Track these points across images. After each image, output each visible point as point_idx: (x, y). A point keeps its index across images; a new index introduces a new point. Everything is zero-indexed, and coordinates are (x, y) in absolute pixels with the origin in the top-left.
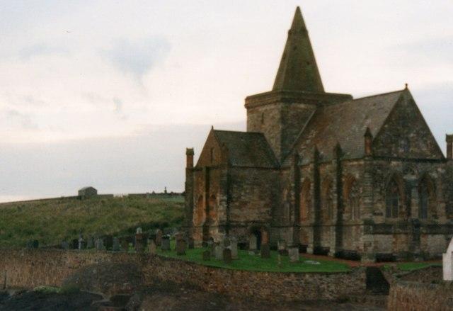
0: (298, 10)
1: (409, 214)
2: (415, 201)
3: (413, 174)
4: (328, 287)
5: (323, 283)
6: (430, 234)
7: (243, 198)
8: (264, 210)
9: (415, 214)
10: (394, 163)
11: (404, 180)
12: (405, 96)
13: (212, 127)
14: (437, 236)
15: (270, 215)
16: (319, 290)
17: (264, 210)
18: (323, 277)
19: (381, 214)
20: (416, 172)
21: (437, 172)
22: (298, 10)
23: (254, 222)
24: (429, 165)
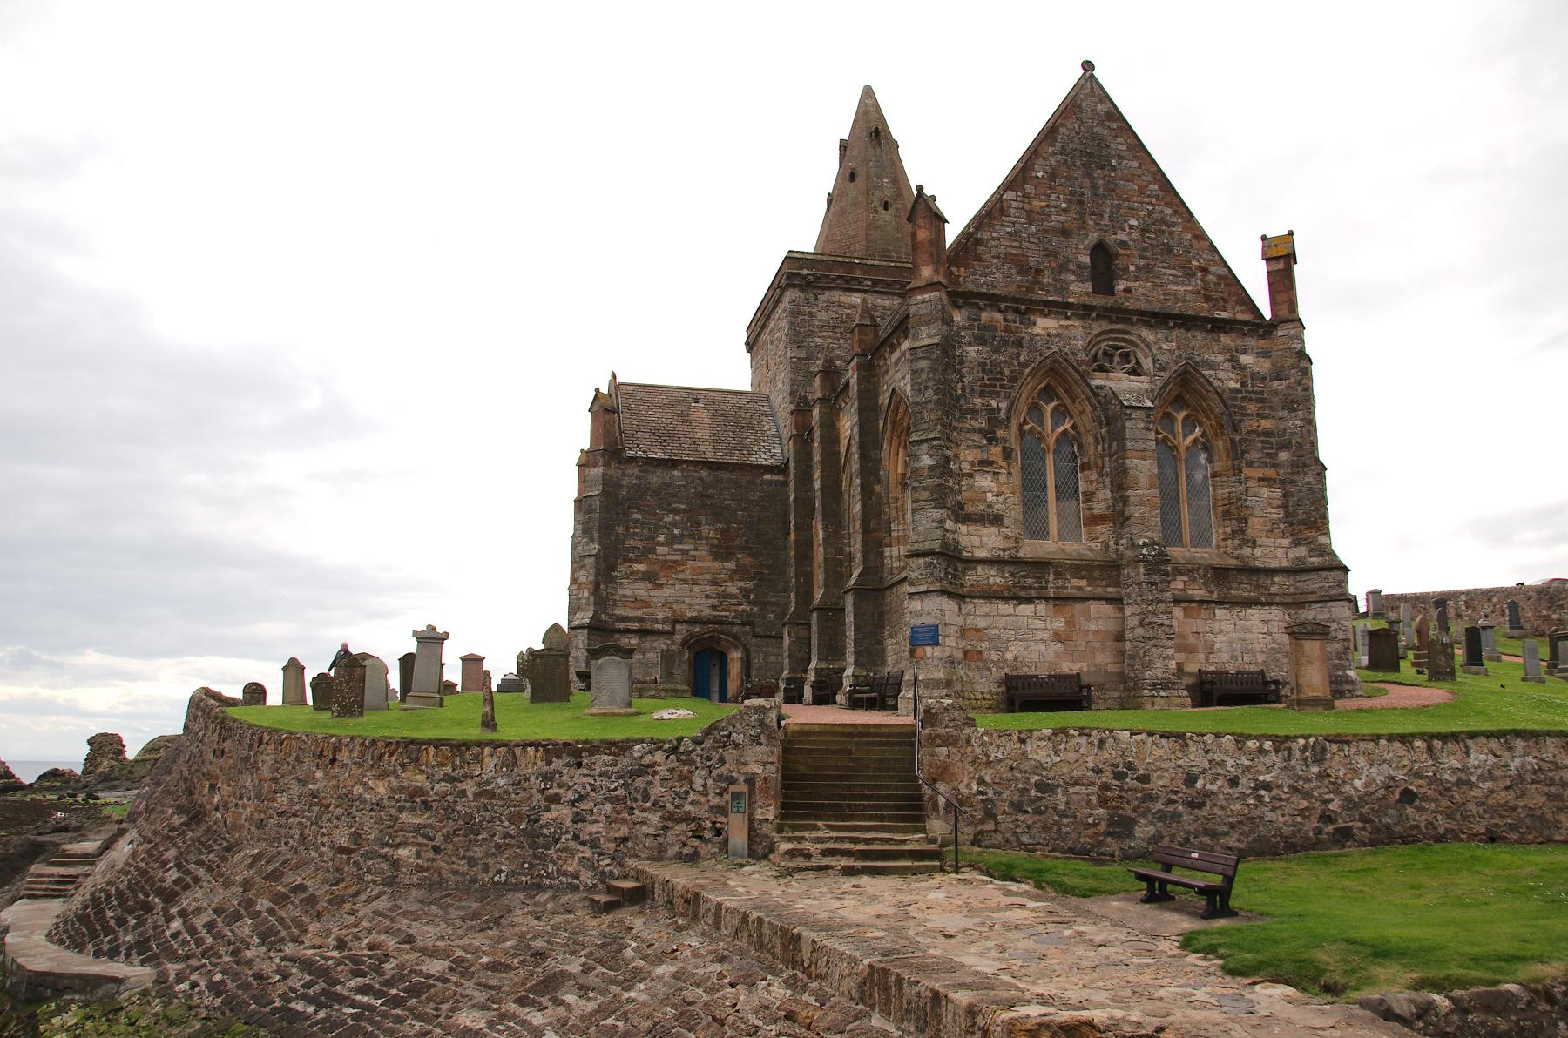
0: (868, 93)
1: (1118, 518)
2: (1143, 468)
3: (1136, 372)
4: (578, 818)
5: (555, 799)
6: (1220, 603)
7: (661, 550)
8: (732, 588)
9: (1146, 525)
10: (1045, 325)
11: (1095, 391)
12: (1087, 104)
13: (614, 376)
14: (1254, 614)
15: (754, 603)
16: (532, 835)
17: (732, 588)
18: (557, 764)
19: (997, 520)
20: (1147, 364)
21: (1236, 366)
22: (868, 93)
23: (694, 621)
24: (1197, 338)
